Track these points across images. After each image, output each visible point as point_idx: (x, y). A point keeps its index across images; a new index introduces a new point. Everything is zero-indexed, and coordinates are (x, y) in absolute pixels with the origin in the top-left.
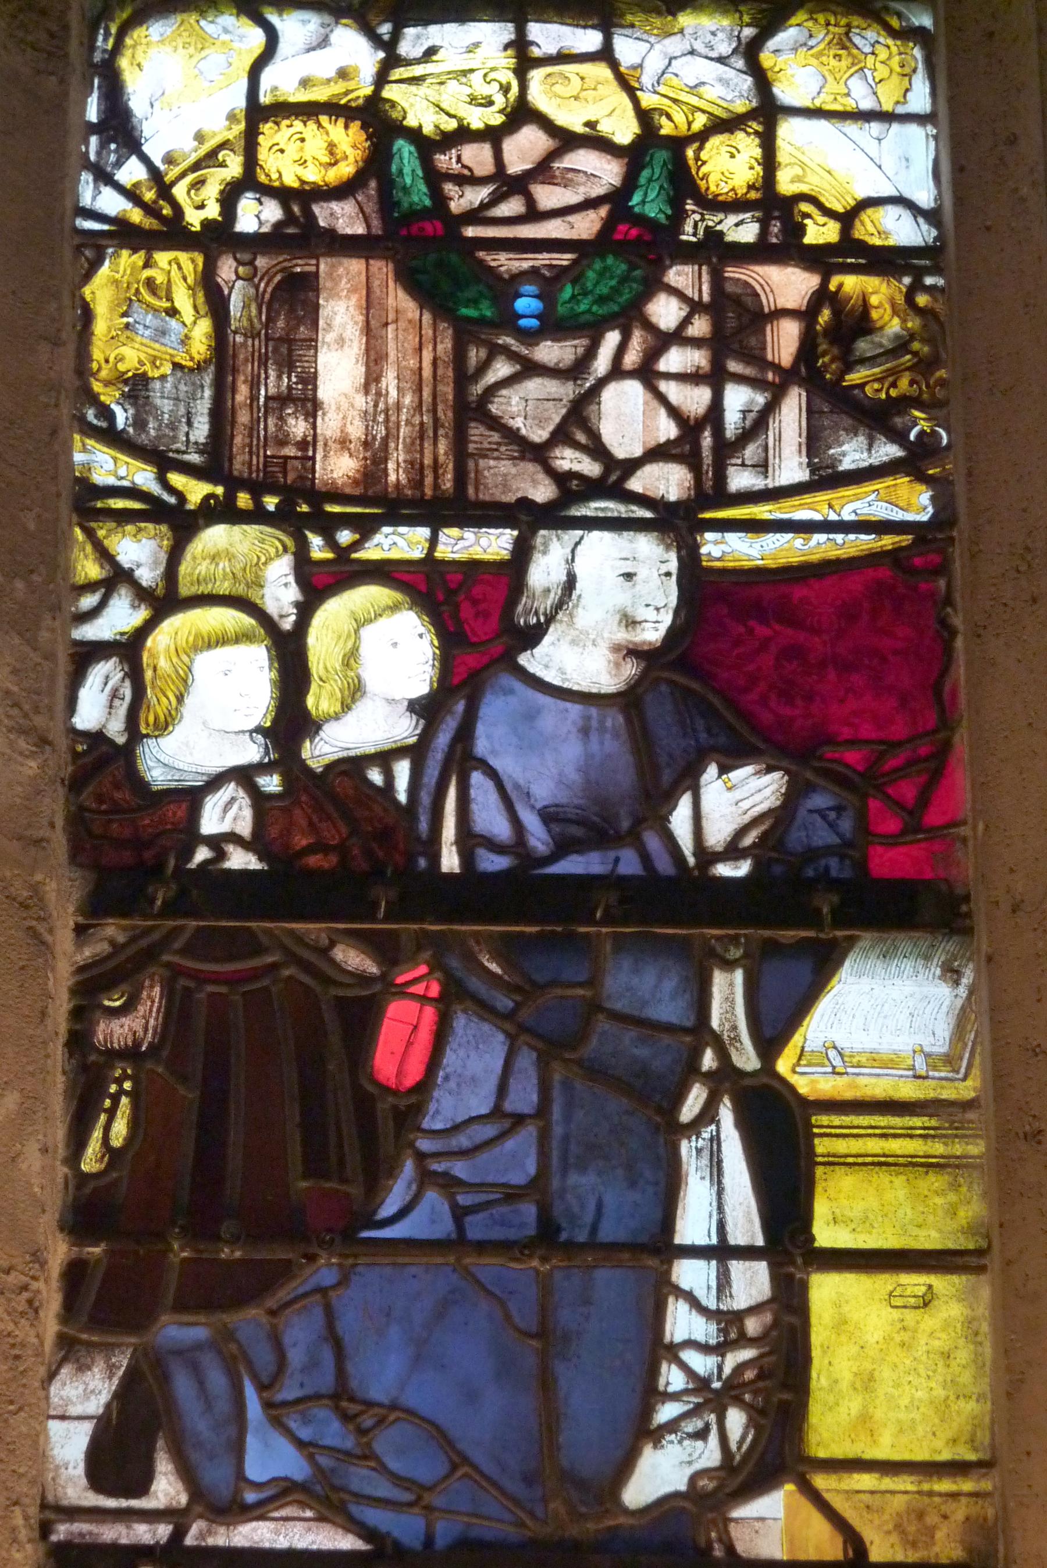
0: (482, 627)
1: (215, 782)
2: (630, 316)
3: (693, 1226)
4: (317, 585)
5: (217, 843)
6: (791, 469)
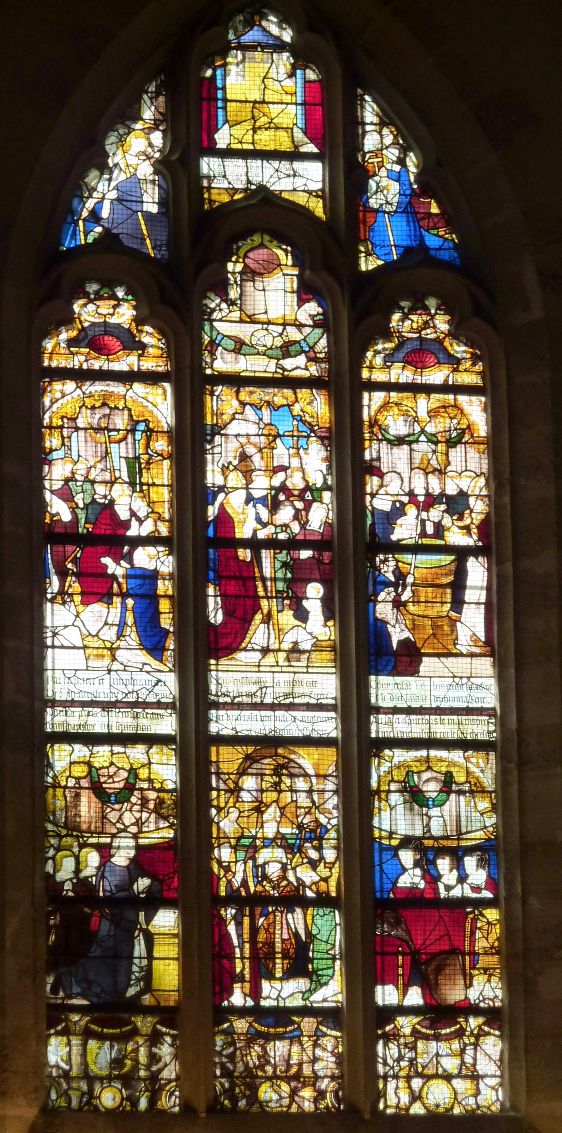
0: (105, 852)
1: (66, 881)
2: (128, 801)
3: (136, 954)
4: (81, 846)
5: (67, 891)
6: (152, 827)
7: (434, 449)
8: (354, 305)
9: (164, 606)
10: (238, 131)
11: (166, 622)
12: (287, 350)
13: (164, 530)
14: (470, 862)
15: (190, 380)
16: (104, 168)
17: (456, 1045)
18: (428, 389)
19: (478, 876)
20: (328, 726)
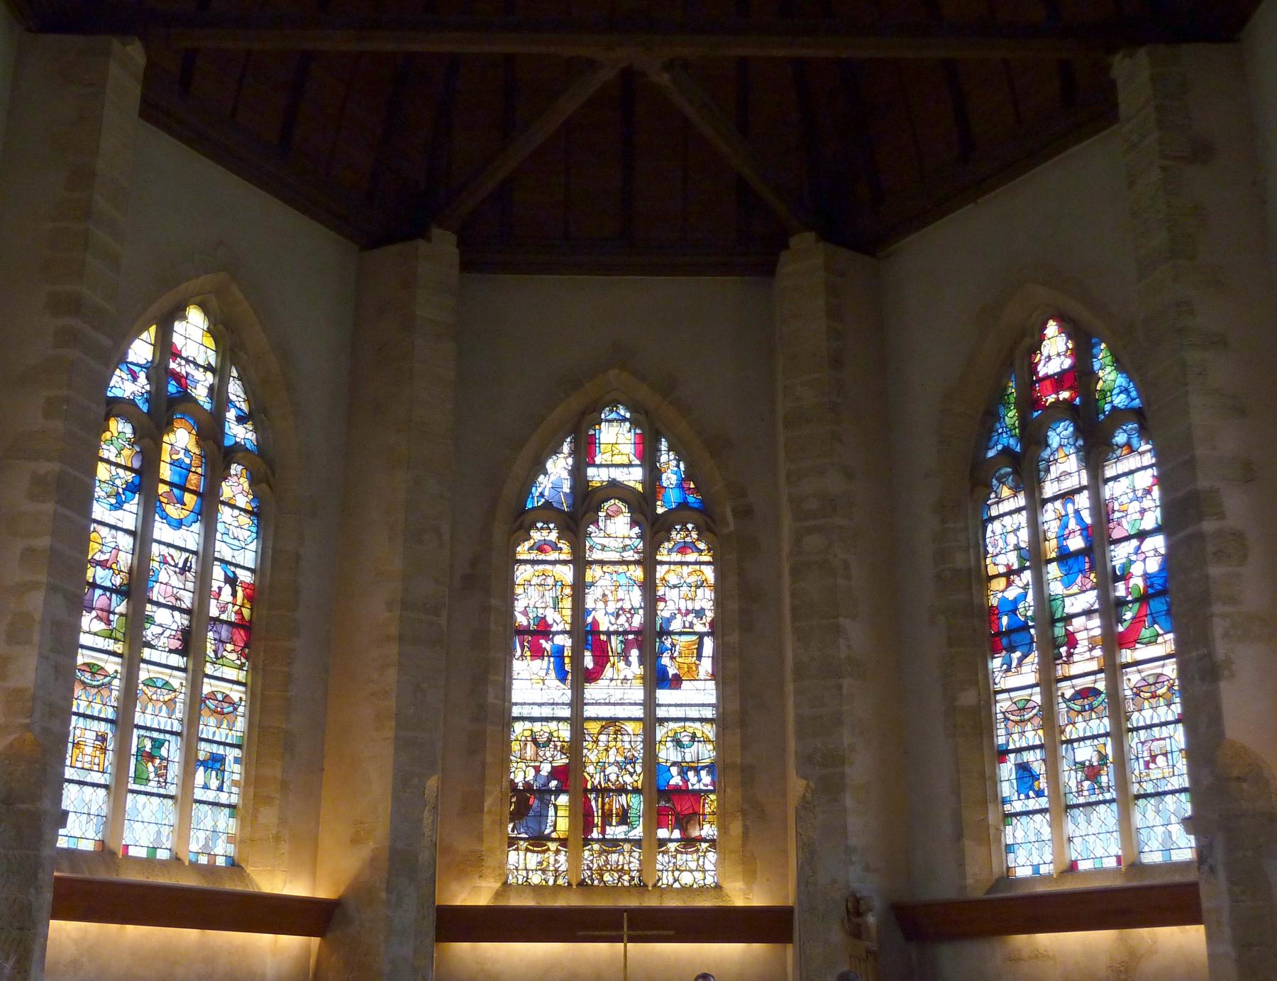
0: (537, 770)
7: (689, 587)
8: (654, 529)
9: (567, 660)
10: (605, 456)
11: (568, 668)
12: (624, 548)
13: (568, 628)
14: (703, 773)
15: (580, 562)
16: (546, 473)
17: (695, 856)
18: (688, 564)
19: (706, 778)
20: (638, 712)
